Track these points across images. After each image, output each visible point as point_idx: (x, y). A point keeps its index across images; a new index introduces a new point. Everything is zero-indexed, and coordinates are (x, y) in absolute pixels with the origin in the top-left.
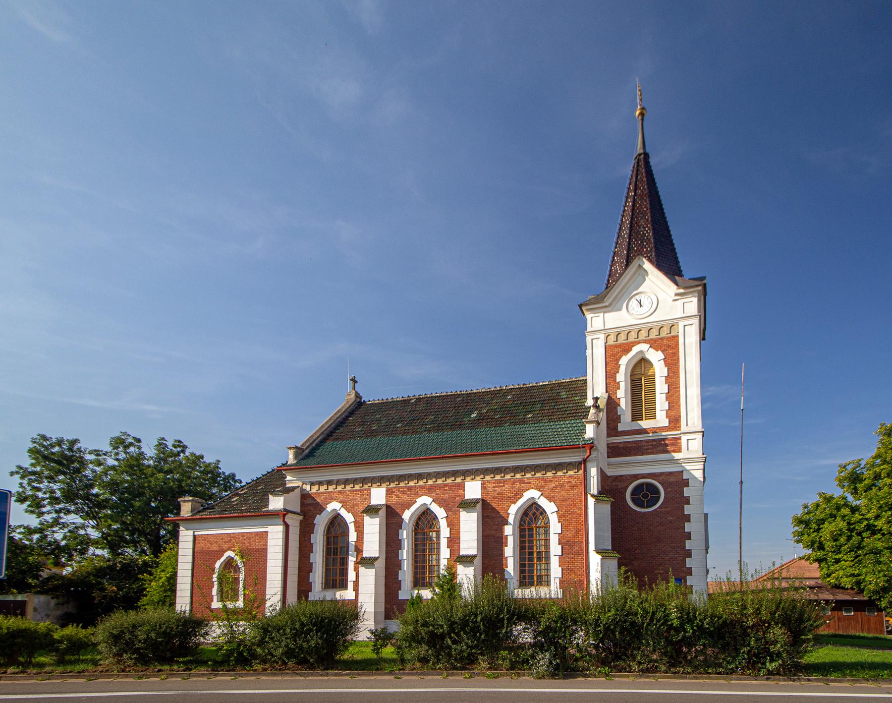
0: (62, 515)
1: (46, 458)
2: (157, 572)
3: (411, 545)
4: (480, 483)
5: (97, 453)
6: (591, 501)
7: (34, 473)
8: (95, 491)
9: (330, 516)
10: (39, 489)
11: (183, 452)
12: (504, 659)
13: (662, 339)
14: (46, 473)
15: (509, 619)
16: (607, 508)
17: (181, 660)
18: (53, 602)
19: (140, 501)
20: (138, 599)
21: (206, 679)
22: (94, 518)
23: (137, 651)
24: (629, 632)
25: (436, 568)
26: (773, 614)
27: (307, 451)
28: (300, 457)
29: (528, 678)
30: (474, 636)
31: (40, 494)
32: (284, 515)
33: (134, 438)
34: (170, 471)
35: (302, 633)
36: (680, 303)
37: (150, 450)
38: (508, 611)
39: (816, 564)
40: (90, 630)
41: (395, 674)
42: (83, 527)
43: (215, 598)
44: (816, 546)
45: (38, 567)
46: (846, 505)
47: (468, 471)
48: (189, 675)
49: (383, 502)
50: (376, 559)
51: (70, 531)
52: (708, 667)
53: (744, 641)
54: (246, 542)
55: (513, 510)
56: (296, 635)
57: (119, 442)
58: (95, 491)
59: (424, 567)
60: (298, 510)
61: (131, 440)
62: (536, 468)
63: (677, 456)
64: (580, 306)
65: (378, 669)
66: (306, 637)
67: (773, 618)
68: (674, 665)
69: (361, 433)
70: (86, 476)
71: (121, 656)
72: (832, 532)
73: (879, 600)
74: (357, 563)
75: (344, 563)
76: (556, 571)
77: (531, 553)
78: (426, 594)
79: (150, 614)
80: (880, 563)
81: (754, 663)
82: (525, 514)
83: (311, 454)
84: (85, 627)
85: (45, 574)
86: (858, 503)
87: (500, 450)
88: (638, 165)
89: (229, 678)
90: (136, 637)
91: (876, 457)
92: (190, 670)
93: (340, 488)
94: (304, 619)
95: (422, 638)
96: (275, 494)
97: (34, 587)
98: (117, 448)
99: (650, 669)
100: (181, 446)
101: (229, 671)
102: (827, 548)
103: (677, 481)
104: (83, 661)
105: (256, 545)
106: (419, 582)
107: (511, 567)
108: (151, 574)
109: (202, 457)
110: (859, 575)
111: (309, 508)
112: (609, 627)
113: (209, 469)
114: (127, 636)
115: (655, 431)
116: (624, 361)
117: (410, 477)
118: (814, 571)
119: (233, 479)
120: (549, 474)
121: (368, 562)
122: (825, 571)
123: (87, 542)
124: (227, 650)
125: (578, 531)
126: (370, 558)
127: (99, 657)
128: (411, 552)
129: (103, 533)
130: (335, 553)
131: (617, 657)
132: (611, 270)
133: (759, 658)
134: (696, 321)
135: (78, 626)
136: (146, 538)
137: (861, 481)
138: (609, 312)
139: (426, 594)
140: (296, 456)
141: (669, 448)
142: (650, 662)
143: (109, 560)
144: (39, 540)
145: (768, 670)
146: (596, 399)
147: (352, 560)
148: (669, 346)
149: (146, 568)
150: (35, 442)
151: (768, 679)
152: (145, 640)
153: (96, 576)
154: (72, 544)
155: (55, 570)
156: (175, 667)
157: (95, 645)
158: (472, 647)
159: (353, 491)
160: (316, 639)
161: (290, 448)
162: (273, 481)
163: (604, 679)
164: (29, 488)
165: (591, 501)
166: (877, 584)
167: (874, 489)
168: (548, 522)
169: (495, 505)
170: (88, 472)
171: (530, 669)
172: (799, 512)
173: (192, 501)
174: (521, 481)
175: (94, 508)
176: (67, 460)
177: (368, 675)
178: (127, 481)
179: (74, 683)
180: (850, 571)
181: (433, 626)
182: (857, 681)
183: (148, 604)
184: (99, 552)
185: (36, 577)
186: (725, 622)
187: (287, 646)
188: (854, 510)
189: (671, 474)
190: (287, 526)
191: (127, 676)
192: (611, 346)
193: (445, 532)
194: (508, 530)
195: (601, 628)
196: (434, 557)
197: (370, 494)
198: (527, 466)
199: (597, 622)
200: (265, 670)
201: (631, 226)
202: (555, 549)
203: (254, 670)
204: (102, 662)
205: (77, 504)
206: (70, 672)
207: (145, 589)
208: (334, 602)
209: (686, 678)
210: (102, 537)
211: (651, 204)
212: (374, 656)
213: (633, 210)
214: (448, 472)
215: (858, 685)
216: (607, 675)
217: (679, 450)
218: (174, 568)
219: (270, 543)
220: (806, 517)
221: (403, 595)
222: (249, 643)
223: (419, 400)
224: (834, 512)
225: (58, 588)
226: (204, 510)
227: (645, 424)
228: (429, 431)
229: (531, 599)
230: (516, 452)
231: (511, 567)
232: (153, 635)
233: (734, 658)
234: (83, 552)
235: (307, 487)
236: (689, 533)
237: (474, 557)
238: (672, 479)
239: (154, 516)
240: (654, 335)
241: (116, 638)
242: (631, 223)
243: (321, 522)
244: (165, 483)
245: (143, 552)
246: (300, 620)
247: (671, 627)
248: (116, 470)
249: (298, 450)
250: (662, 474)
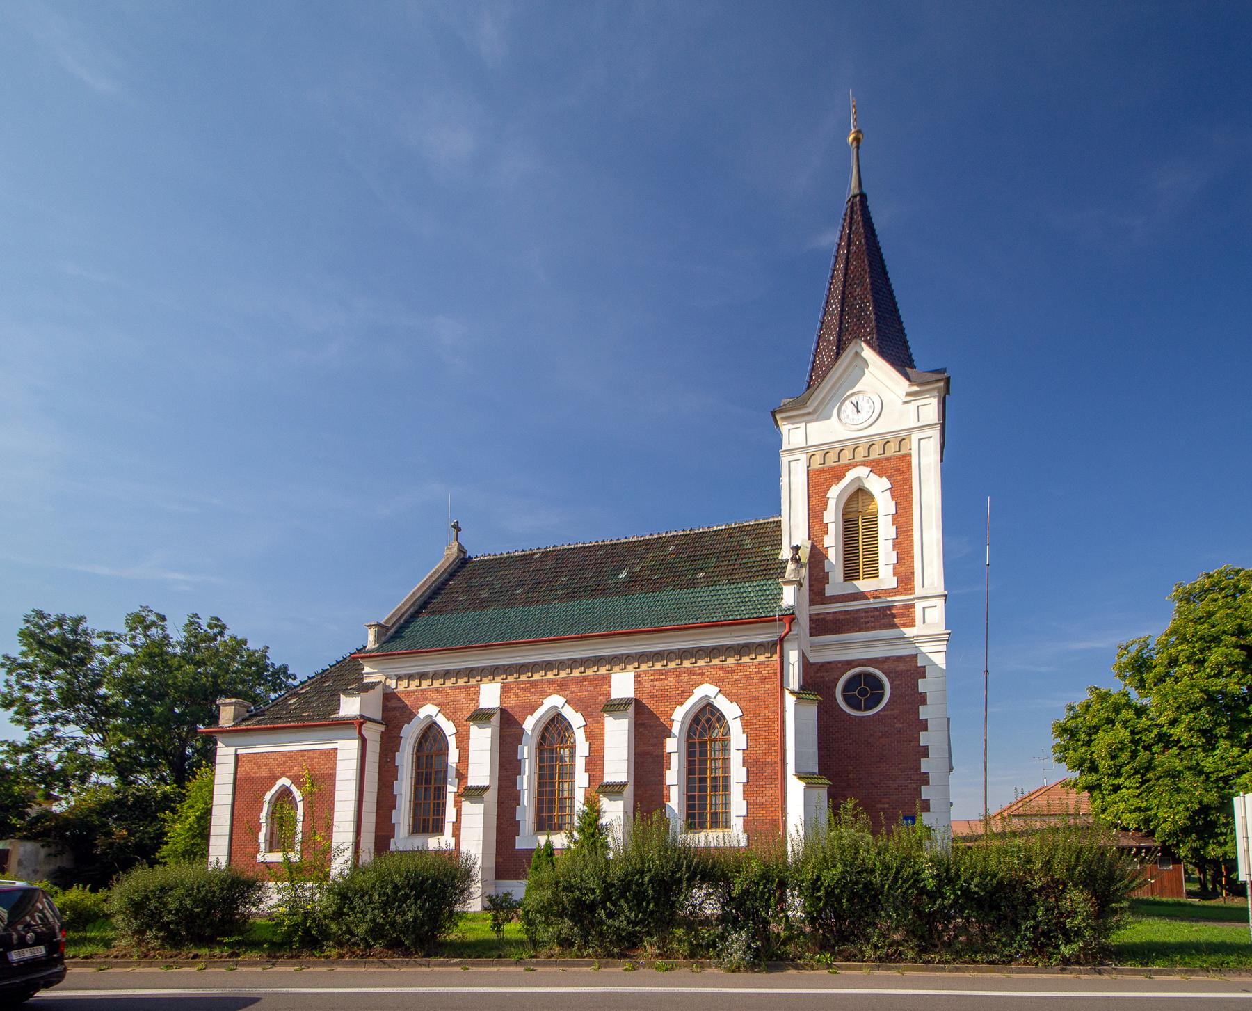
0: (58, 726)
1: (41, 644)
2: (183, 808)
3: (535, 769)
4: (632, 674)
5: (108, 636)
6: (790, 700)
7: (24, 666)
8: (103, 691)
10: (29, 689)
11: (221, 634)
12: (680, 941)
13: (887, 459)
14: (41, 665)
15: (690, 880)
16: (812, 711)
17: (226, 940)
18: (43, 852)
19: (161, 705)
20: (156, 848)
21: (259, 969)
22: (100, 730)
23: (165, 926)
24: (862, 899)
25: (568, 802)
26: (1070, 870)
27: (393, 630)
28: (384, 639)
29: (715, 970)
30: (639, 905)
31: (31, 696)
32: (361, 725)
33: (158, 615)
34: (201, 663)
35: (395, 900)
37: (177, 633)
38: (689, 867)
39: (1086, 793)
40: (101, 894)
41: (525, 964)
42: (85, 743)
44: (1086, 766)
45: (26, 800)
46: (1128, 705)
47: (615, 657)
48: (237, 963)
49: (497, 704)
50: (485, 789)
51: (68, 750)
52: (976, 953)
53: (1027, 911)
55: (679, 715)
56: (386, 903)
57: (138, 621)
58: (103, 691)
59: (551, 801)
60: (379, 716)
61: (153, 618)
62: (712, 652)
63: (908, 632)
64: (773, 414)
65: (500, 956)
66: (400, 906)
67: (1070, 877)
68: (925, 950)
69: (466, 605)
70: (92, 670)
71: (143, 933)
72: (1110, 746)
73: (1177, 846)
74: (458, 796)
75: (440, 794)
76: (738, 806)
77: (703, 780)
78: (559, 840)
79: (173, 871)
80: (1178, 790)
81: (1043, 946)
82: (696, 720)
83: (398, 635)
84: (94, 890)
85: (34, 811)
86: (1145, 701)
87: (663, 625)
88: (852, 212)
89: (292, 969)
90: (165, 905)
91: (1171, 633)
92: (238, 955)
93: (437, 684)
94: (398, 879)
95: (564, 908)
96: (349, 693)
97: (20, 829)
98: (135, 629)
99: (891, 957)
100: (218, 625)
101: (292, 957)
102: (1101, 770)
103: (909, 670)
104: (90, 940)
105: (321, 768)
106: (545, 823)
107: (675, 801)
108: (174, 811)
109: (245, 642)
110: (1147, 809)
111: (394, 713)
112: (832, 891)
113: (253, 659)
114: (153, 903)
115: (877, 595)
116: (834, 492)
118: (1084, 803)
119: (285, 673)
120: (731, 661)
121: (475, 794)
122: (1098, 803)
123: (88, 766)
124: (289, 926)
126: (477, 788)
127: (112, 934)
128: (534, 777)
129: (111, 752)
130: (428, 781)
131: (843, 938)
132: (814, 361)
133: (1050, 939)
134: (935, 433)
135: (84, 887)
136: (167, 760)
137: (1150, 669)
138: (817, 420)
139: (559, 840)
140: (378, 637)
142: (890, 945)
143: (118, 792)
144: (27, 763)
145: (1064, 957)
146: (796, 549)
147: (451, 789)
148: (897, 470)
149: (167, 803)
150: (28, 621)
151: (1062, 970)
152: (177, 910)
153: (100, 814)
154: (71, 768)
155: (45, 806)
156: (217, 951)
157: (108, 916)
158: (635, 923)
159: (455, 688)
160: (409, 913)
161: (370, 626)
162: (344, 675)
163: (825, 972)
164: (17, 687)
165: (790, 700)
166: (1174, 822)
167: (1168, 681)
168: (728, 733)
169: (653, 708)
170: (94, 664)
171: (718, 956)
172: (1062, 717)
173: (235, 704)
174: (691, 672)
175: (100, 716)
176: (68, 647)
177: (487, 964)
178: (145, 678)
179: (79, 974)
180: (1136, 803)
181: (580, 890)
182: (1193, 972)
183: (169, 856)
184: (104, 779)
185: (21, 815)
186: (1000, 883)
187: (373, 920)
188: (1140, 712)
189: (900, 659)
190: (363, 741)
191: (151, 965)
193: (582, 748)
194: (672, 745)
195: (822, 893)
196: (566, 785)
197: (478, 692)
198: (700, 649)
199: (816, 884)
200: (342, 956)
201: (843, 298)
202: (738, 774)
203: (327, 957)
204: (116, 943)
205: (78, 710)
206: (74, 957)
207: (165, 834)
208: (423, 852)
209: (944, 970)
210: (109, 757)
211: (870, 265)
212: (493, 936)
213: (845, 275)
214: (588, 659)
215: (1193, 978)
216: (829, 966)
217: (912, 624)
218: (206, 803)
219: (340, 765)
220: (1071, 724)
221: (521, 843)
222: (318, 915)
223: (545, 554)
224: (1112, 716)
225: (52, 832)
226: (252, 717)
227: (863, 585)
228: (561, 599)
229: (717, 848)
230: (685, 629)
231: (675, 801)
232: (188, 903)
233: (1012, 938)
234: (83, 780)
236: (926, 748)
237: (624, 785)
238: (902, 667)
239: (178, 728)
240: (876, 454)
241: (137, 907)
242: (843, 292)
243: (410, 734)
244: (195, 679)
245: (163, 779)
246: (392, 882)
247: (923, 891)
248: (131, 661)
249: (381, 629)
250: (887, 659)
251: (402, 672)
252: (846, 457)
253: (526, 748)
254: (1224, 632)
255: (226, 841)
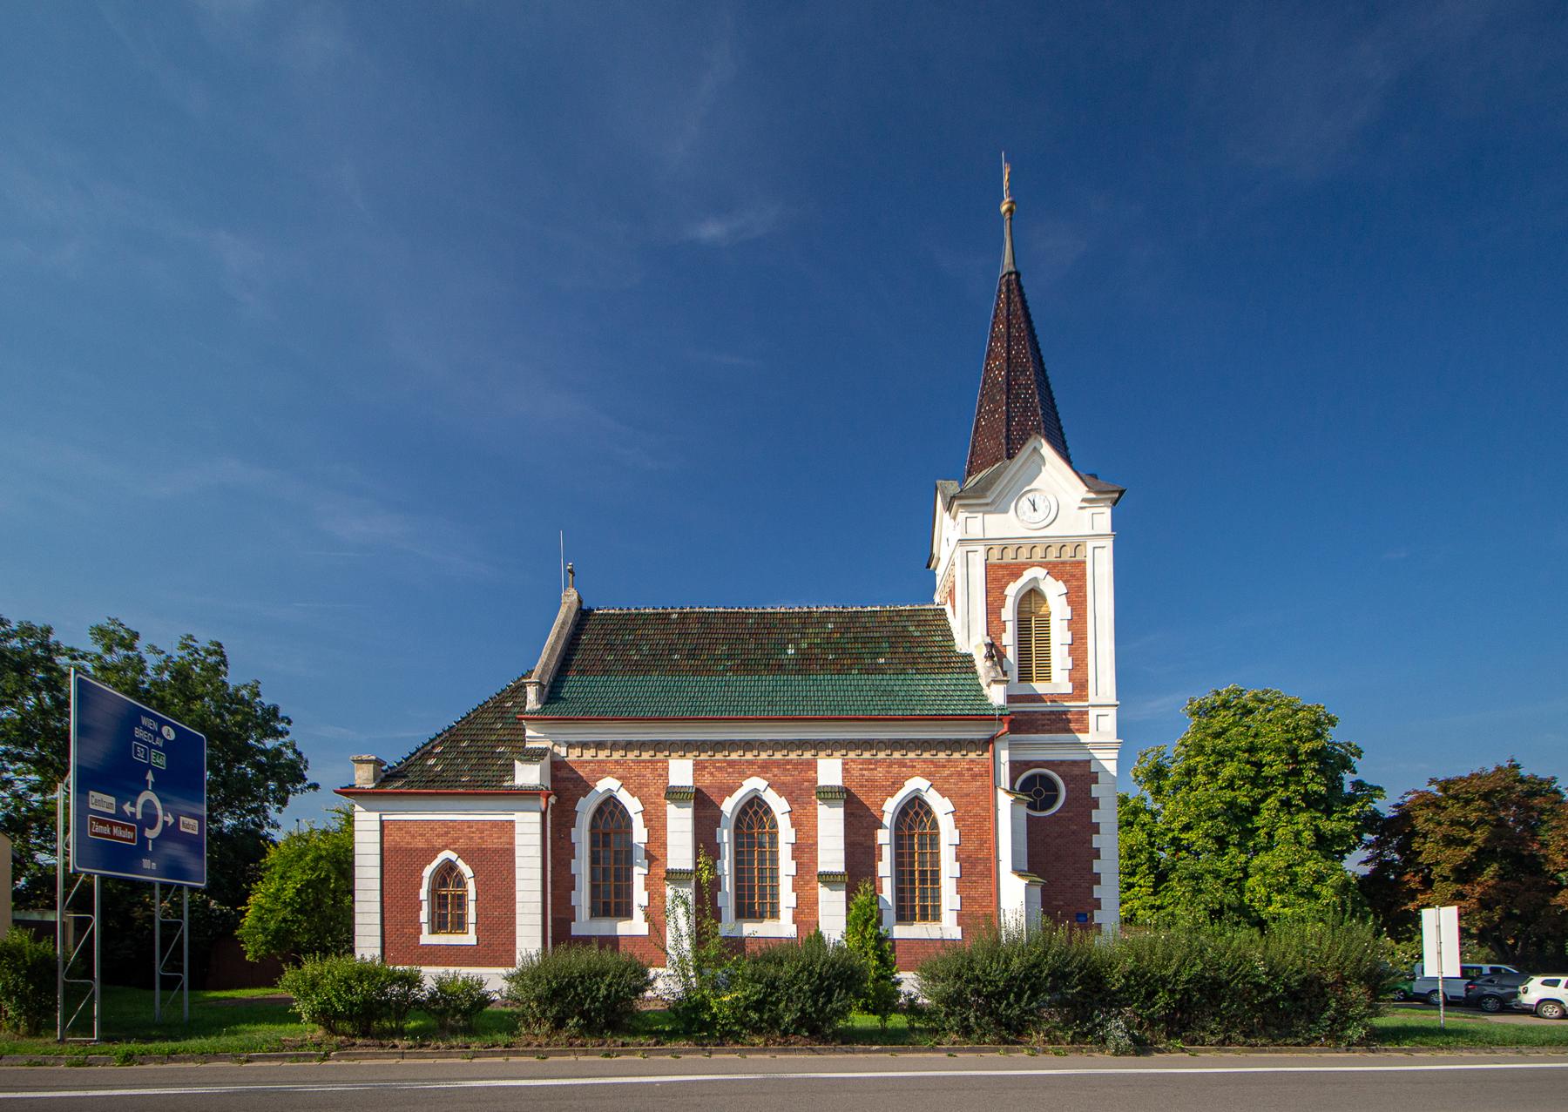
9: (599, 801)
13: (1063, 563)
36: (1088, 512)
43: (425, 928)
47: (822, 742)
54: (476, 836)
55: (891, 806)
63: (1083, 737)
76: (949, 898)
93: (617, 755)
103: (1083, 775)
105: (493, 842)
107: (887, 893)
111: (565, 787)
115: (1054, 698)
117: (732, 745)
120: (942, 755)
125: (982, 842)
137: (1166, 777)
141: (1072, 726)
147: (639, 873)
148: (1073, 576)
169: (863, 798)
174: (902, 764)
188: (1154, 815)
189: (1074, 763)
192: (994, 565)
193: (786, 835)
194: (884, 837)
197: (667, 768)
198: (911, 741)
221: (577, 929)
224: (1131, 819)
235: (563, 751)
236: (1098, 850)
238: (1076, 771)
240: (1052, 556)
243: (586, 808)
247: (1257, 985)
250: (1062, 762)
251: (573, 739)
252: (1023, 556)
253: (726, 832)
254: (1238, 748)
255: (377, 920)
